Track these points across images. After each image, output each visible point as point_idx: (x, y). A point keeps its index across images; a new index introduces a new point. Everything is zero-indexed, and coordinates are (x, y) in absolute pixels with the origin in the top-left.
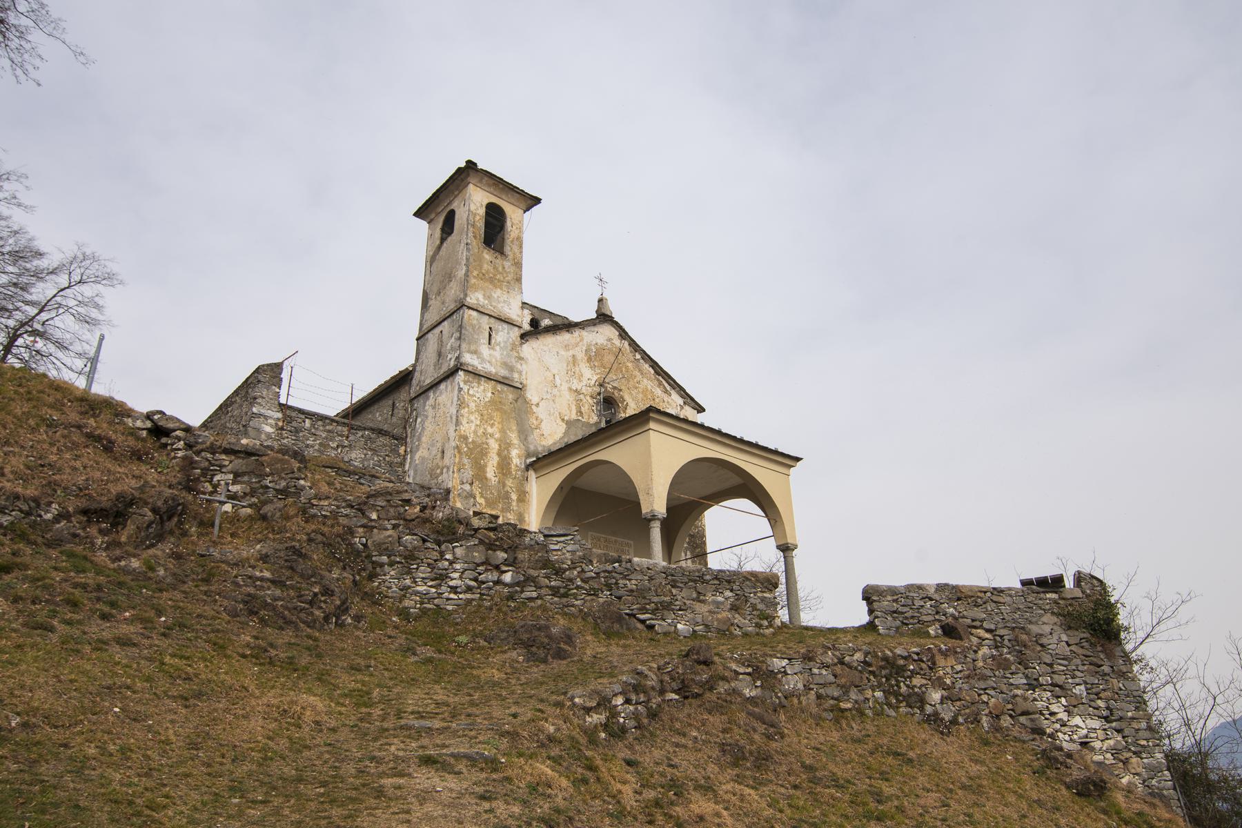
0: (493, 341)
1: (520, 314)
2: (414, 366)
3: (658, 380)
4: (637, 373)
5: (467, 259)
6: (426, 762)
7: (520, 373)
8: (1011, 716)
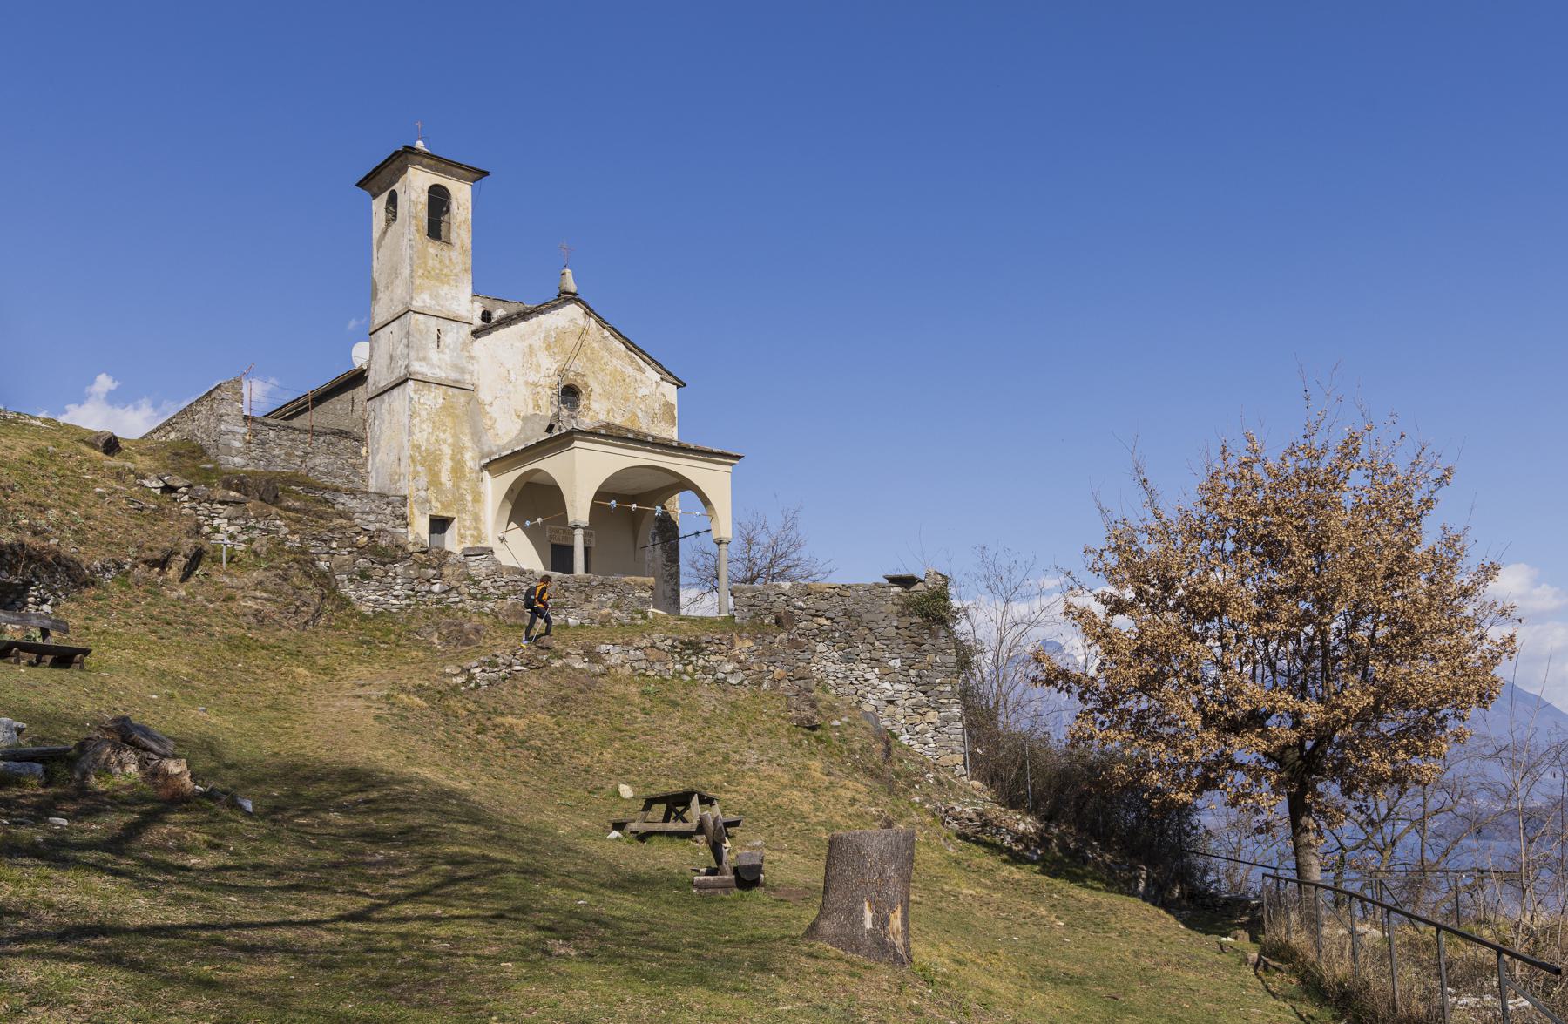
0: (442, 344)
1: (469, 308)
3: (630, 357)
5: (411, 259)
7: (472, 373)
8: (790, 680)
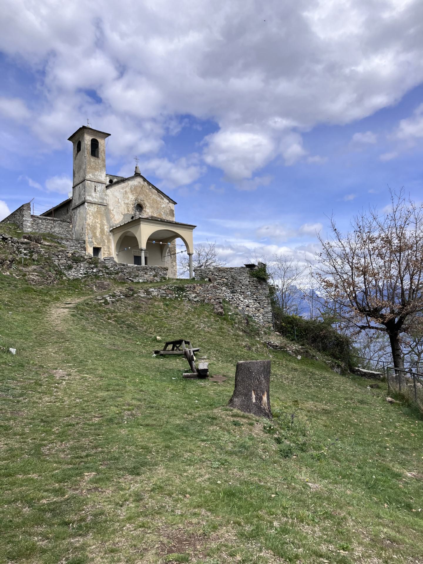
0: (96, 190)
2: (72, 197)
4: (150, 193)
6: (26, 291)
